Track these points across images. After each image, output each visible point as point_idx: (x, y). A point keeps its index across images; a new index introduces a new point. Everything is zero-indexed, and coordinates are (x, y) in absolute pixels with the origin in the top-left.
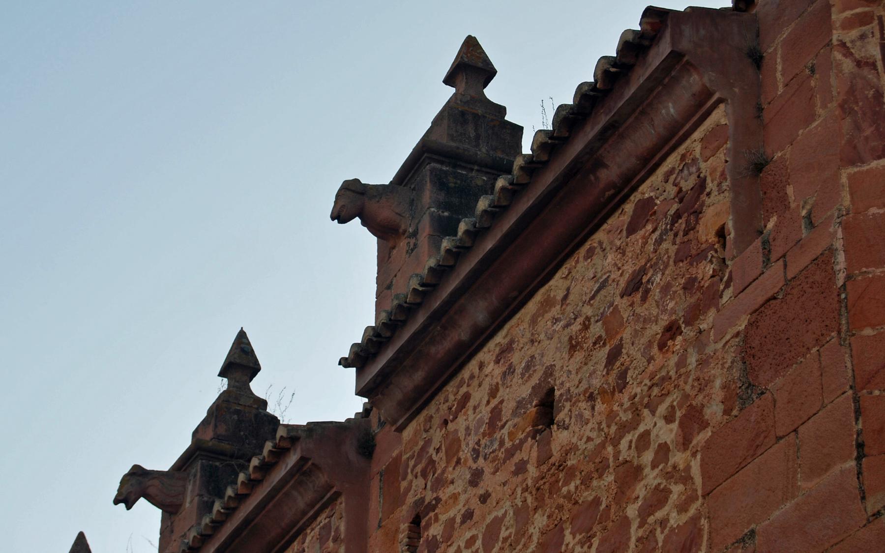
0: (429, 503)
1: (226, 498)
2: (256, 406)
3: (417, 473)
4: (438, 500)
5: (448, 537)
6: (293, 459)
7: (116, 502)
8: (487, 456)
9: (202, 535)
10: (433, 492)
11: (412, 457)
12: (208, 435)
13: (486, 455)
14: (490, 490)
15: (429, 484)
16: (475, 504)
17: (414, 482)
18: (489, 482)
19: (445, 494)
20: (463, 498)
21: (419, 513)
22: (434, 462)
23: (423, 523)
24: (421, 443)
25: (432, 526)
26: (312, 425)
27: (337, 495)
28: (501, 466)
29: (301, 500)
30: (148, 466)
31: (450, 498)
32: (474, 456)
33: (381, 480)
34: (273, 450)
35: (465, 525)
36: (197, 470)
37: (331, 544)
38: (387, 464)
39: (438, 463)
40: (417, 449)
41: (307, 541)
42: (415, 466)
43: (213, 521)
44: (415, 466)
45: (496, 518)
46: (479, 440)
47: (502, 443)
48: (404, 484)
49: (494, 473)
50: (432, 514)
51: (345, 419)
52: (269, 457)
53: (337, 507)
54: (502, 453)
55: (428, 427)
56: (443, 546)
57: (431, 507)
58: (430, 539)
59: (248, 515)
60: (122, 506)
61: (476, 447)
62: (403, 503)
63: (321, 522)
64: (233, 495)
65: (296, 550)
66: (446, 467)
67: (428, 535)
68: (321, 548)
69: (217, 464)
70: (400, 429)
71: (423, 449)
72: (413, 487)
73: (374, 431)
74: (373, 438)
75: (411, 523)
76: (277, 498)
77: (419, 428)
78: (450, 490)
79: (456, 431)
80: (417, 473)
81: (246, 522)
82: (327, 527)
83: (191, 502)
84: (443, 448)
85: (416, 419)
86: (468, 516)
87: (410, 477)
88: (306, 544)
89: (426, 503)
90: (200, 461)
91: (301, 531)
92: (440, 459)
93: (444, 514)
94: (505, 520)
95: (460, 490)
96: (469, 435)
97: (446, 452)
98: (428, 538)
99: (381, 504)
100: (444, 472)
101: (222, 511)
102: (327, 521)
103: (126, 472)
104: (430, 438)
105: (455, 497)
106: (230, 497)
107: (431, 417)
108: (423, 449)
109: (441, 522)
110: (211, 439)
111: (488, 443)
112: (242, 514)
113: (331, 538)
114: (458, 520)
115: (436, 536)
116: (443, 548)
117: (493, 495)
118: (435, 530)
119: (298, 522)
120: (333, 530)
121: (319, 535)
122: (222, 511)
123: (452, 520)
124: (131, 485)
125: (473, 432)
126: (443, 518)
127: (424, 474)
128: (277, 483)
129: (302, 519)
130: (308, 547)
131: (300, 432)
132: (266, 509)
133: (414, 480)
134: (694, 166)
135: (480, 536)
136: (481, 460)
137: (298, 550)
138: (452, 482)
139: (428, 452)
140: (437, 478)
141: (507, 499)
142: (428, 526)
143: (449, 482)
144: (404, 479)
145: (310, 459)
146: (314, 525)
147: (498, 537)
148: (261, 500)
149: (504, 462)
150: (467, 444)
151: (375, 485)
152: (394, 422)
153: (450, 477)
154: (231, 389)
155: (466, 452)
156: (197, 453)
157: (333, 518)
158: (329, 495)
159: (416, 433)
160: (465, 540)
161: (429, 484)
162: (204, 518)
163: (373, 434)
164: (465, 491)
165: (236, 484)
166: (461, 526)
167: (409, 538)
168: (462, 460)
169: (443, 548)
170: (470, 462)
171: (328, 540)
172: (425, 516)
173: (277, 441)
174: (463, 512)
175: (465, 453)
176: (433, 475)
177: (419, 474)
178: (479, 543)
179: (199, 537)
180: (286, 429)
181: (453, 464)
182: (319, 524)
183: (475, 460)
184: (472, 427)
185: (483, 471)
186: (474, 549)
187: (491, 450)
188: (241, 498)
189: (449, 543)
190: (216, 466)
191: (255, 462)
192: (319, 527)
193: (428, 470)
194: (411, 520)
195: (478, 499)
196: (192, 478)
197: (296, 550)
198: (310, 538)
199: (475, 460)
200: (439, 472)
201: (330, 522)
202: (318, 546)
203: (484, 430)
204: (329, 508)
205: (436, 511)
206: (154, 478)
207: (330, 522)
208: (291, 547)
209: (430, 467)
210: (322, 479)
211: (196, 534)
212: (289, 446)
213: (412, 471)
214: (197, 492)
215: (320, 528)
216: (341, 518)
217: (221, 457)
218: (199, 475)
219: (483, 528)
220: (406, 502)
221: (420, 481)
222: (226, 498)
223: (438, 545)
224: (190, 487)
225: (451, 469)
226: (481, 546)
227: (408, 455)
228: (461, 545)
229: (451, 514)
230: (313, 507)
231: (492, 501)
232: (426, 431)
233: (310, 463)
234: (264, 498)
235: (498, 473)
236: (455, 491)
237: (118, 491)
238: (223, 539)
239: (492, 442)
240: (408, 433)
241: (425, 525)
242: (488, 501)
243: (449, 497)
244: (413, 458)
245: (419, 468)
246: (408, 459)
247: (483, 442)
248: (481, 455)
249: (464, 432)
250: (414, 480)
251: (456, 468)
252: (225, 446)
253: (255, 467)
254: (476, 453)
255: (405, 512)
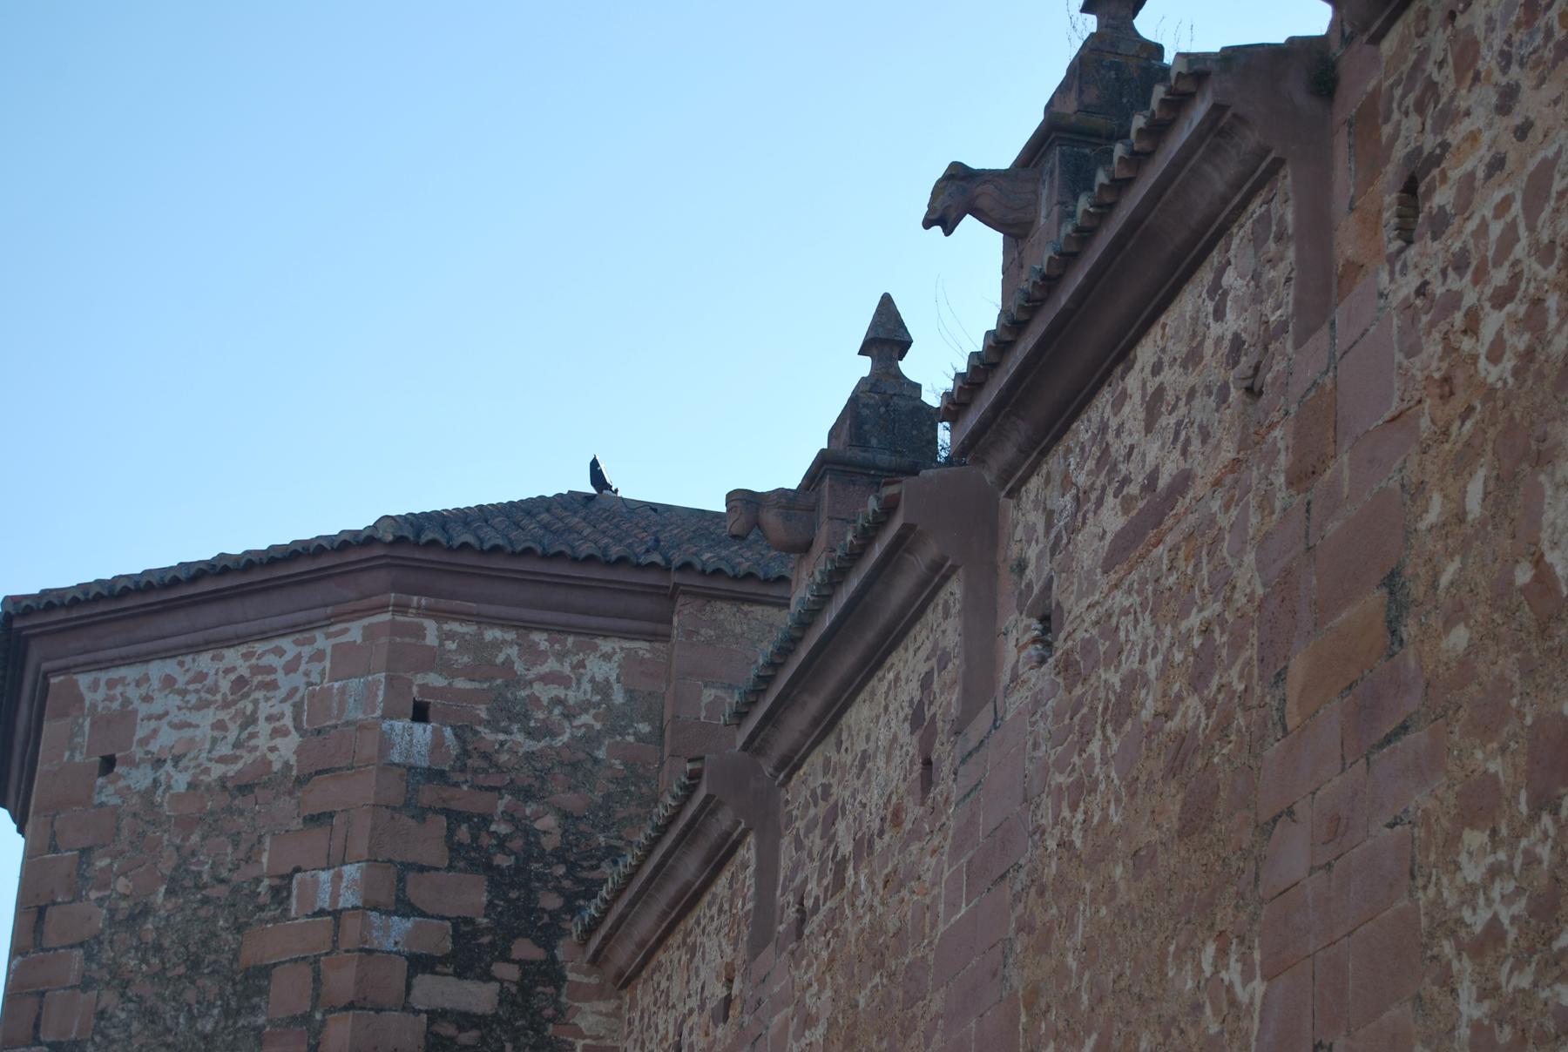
0: (1431, 154)
1: (1096, 189)
2: (1144, 55)
3: (1408, 107)
4: (1445, 146)
5: (1465, 203)
6: (1199, 110)
7: (928, 224)
8: (1525, 60)
9: (1061, 254)
10: (1435, 135)
11: (1397, 83)
12: (1070, 106)
13: (1522, 58)
14: (1532, 116)
15: (1429, 122)
16: (1508, 143)
17: (1403, 122)
18: (1532, 103)
19: (1454, 136)
20: (1486, 137)
21: (1413, 172)
22: (1435, 84)
23: (1422, 188)
24: (1413, 57)
25: (1437, 192)
26: (1229, 52)
27: (1279, 163)
28: (1549, 73)
29: (1218, 179)
30: (975, 164)
31: (1465, 139)
32: (1503, 64)
33: (1349, 133)
34: (1168, 97)
35: (1492, 180)
36: (1054, 164)
37: (1272, 246)
38: (1358, 106)
39: (1443, 85)
40: (1405, 68)
41: (1233, 247)
42: (1404, 96)
43: (1077, 229)
44: (1404, 96)
45: (1545, 160)
46: (1510, 36)
47: (1549, 33)
48: (1387, 130)
49: (1538, 87)
50: (1436, 172)
51: (1286, 38)
52: (1160, 110)
53: (1279, 184)
54: (1550, 51)
55: (1423, 28)
56: (1457, 221)
57: (1435, 160)
58: (1434, 212)
59: (1134, 211)
60: (937, 230)
61: (1506, 48)
62: (1387, 160)
63: (1254, 212)
64: (1106, 181)
65: (1216, 264)
66: (1455, 90)
67: (1430, 207)
68: (1256, 254)
69: (1087, 151)
70: (1376, 39)
71: (1417, 66)
72: (1403, 133)
73: (1334, 54)
74: (1334, 66)
75: (1402, 191)
76: (1180, 177)
77: (1407, 32)
78: (1465, 126)
79: (1470, 27)
80: (1408, 107)
81: (1134, 223)
82: (1264, 220)
83: (1048, 216)
84: (1450, 60)
85: (1403, 17)
86: (1497, 164)
87: (1396, 116)
88: (1232, 252)
89: (1425, 153)
90: (1058, 148)
91: (1223, 231)
92: (1445, 78)
93: (1456, 168)
94: (1560, 161)
95: (1480, 124)
96: (1493, 29)
97: (1456, 66)
98: (1431, 212)
99: (1353, 173)
100: (1452, 98)
101: (1091, 210)
102: (1263, 209)
103: (940, 176)
104: (1426, 46)
105: (1473, 137)
106: (1102, 186)
107: (1428, 10)
108: (1417, 66)
109: (1451, 182)
110: (1075, 113)
111: (1525, 38)
112: (1124, 212)
113: (1272, 235)
114: (1480, 174)
115: (1444, 206)
116: (1456, 224)
117: (1538, 123)
118: (1443, 197)
119: (1217, 216)
120: (1274, 222)
121: (1252, 233)
122: (1091, 210)
123: (1471, 176)
124: (950, 195)
125: (1498, 24)
126: (1454, 175)
127: (1420, 108)
128: (1177, 153)
129: (1223, 209)
130: (1236, 257)
131: (1209, 63)
132: (1164, 199)
133: (1404, 121)
134: (1435, 211)
135: (1519, 197)
136: (1515, 69)
137: (1220, 262)
138: (1468, 113)
139: (1424, 71)
140: (1441, 111)
141: (1562, 126)
142: (1431, 190)
143: (1461, 114)
144: (1387, 120)
145: (1229, 107)
146: (1242, 219)
147: (1549, 192)
148: (1153, 187)
149: (1555, 64)
150: (1490, 47)
151: (1342, 141)
152: (1365, 28)
153: (1463, 105)
154: (1104, 30)
155: (1488, 59)
156: (1053, 136)
157: (1273, 204)
158: (1264, 165)
159: (1403, 42)
160: (1493, 205)
161: (1429, 122)
162: (1064, 224)
163: (1334, 59)
164: (1490, 125)
165: (1111, 162)
166: (1485, 183)
167: (1399, 216)
168: (1483, 74)
169: (1456, 224)
170: (1497, 76)
171: (1267, 239)
172: (1423, 178)
173: (1173, 82)
174: (1487, 159)
175: (1488, 60)
176: (1435, 107)
177: (1411, 108)
178: (1517, 207)
179: (1057, 257)
180: (1185, 60)
181: (1468, 82)
182: (1251, 217)
183: (1505, 70)
184: (1497, 16)
185: (1518, 86)
186: (1509, 218)
187: (1531, 49)
188: (1120, 186)
189: (1467, 215)
190: (1085, 155)
191: (1139, 122)
192: (1251, 221)
193: (1426, 100)
194: (1401, 186)
195: (1512, 135)
196: (1048, 177)
197: (1216, 264)
198: (1238, 241)
199: (1505, 70)
200: (1444, 99)
201: (1268, 210)
202: (1250, 251)
203: (1518, 18)
204: (1266, 189)
205: (1443, 166)
206: (985, 182)
207: (1268, 210)
208: (1208, 260)
209: (1429, 94)
210: (1251, 139)
211: (1052, 254)
212: (1193, 89)
213: (1400, 105)
214: (1055, 198)
215: (1253, 223)
216: (1286, 202)
217: (1093, 140)
218: (1057, 171)
219: (1522, 180)
220: (1392, 159)
221: (1414, 121)
222: (1096, 189)
223: (1448, 221)
224: (1045, 192)
225: (1464, 92)
226: (1520, 211)
227: (1391, 81)
228: (1486, 214)
229: (1468, 166)
230: (1240, 188)
231: (1536, 134)
232: (1420, 35)
233: (1229, 114)
234: (1157, 180)
235: (1544, 86)
236: (1474, 128)
237: (929, 206)
238: (1097, 256)
239: (1531, 37)
240: (1389, 45)
241: (1425, 191)
242: (1530, 135)
243: (1463, 138)
244: (1399, 85)
245: (1410, 100)
246: (1392, 87)
247: (1516, 38)
248: (1514, 60)
249: (1483, 27)
250: (1404, 121)
251: (1473, 89)
252: (1098, 121)
253: (1140, 131)
254: (1506, 58)
255: (1391, 174)
